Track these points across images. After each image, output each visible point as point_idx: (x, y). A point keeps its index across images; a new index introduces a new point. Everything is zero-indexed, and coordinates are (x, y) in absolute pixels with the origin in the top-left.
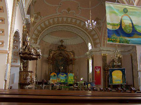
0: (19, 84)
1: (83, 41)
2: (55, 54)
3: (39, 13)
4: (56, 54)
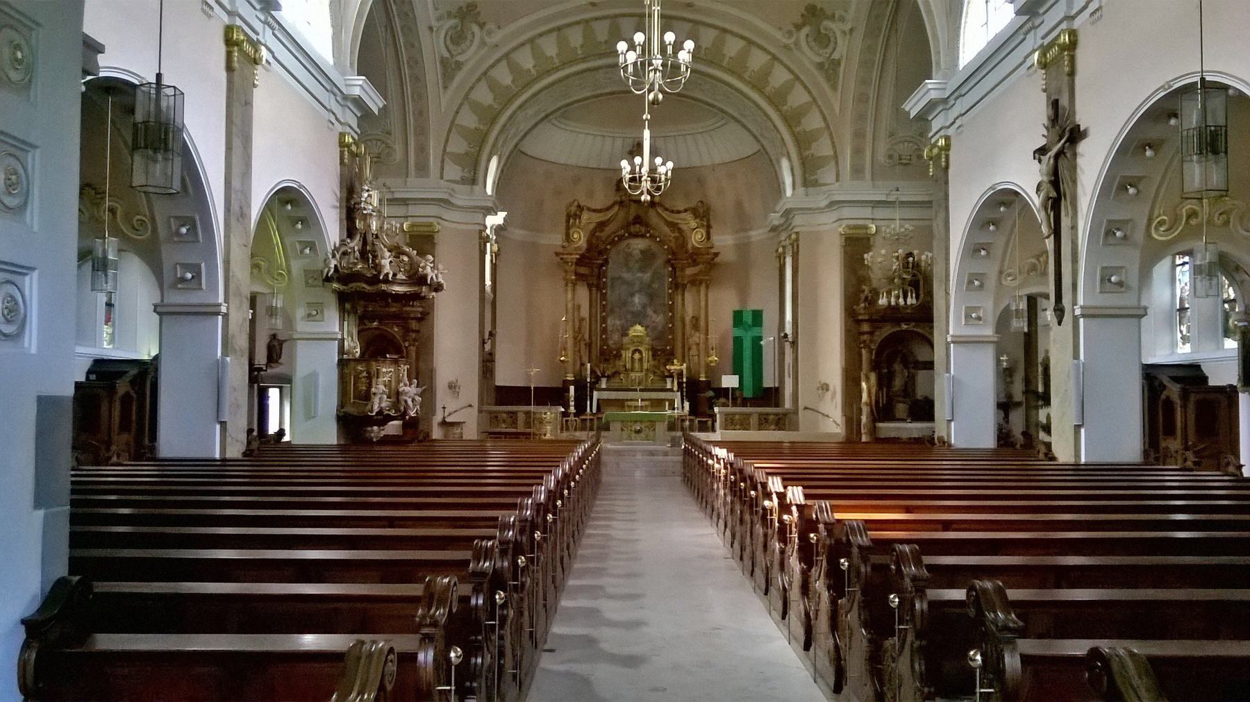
1: (756, 147)
2: (601, 225)
3: (471, 7)
4: (609, 230)
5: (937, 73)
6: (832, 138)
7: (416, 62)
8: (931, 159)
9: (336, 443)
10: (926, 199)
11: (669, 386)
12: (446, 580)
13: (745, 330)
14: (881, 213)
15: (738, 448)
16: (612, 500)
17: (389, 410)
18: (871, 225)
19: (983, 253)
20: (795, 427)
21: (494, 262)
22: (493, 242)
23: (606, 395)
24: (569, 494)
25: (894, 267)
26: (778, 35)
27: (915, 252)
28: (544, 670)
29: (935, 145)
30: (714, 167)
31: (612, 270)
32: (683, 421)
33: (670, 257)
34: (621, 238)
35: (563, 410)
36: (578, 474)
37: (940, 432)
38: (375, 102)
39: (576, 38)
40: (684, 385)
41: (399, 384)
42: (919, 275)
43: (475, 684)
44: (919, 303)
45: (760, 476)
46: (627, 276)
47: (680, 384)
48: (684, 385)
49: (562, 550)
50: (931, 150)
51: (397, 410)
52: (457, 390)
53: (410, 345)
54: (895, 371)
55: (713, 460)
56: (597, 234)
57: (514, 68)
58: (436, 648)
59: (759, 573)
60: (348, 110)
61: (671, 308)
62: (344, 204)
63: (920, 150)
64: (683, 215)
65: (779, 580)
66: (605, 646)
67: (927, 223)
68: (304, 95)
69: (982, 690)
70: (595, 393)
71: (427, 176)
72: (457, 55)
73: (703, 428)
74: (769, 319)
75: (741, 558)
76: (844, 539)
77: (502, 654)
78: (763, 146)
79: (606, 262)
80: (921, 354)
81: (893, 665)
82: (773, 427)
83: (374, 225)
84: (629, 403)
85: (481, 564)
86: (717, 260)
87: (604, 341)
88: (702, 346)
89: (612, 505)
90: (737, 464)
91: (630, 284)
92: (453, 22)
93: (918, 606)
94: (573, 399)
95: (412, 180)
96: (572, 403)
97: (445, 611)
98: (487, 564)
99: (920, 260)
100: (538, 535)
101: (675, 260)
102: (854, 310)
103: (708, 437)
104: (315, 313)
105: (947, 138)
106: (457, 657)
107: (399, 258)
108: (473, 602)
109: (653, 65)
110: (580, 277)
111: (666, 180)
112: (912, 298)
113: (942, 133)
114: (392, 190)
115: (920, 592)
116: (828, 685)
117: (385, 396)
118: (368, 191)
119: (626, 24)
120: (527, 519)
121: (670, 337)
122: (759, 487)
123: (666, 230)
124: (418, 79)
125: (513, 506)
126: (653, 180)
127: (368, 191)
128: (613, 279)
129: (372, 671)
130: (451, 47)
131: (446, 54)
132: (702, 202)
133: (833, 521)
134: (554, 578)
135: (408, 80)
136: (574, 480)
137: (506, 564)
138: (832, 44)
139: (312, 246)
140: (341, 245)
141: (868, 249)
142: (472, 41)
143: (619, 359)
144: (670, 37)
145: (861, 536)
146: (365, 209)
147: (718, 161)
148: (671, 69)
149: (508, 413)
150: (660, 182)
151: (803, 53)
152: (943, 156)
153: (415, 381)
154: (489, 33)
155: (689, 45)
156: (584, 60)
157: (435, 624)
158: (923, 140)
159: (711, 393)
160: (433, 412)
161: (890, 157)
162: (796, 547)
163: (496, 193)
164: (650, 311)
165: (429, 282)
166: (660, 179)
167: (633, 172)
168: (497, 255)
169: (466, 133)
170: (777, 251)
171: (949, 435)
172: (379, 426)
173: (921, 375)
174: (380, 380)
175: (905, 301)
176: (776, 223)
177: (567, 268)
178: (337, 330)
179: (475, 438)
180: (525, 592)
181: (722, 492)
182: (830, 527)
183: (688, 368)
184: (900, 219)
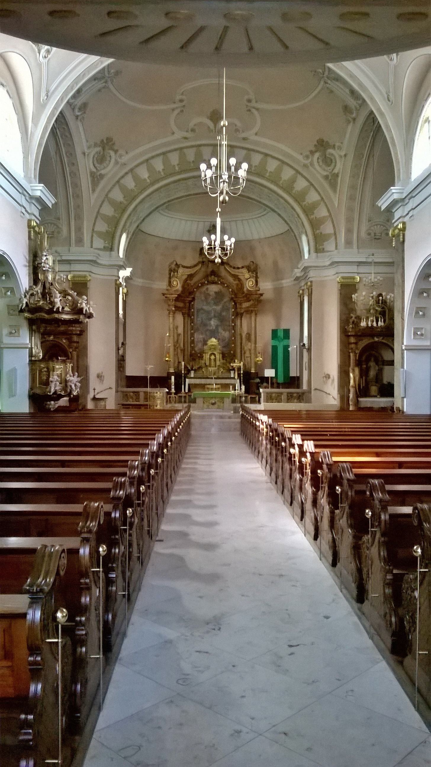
0: (29, 399)
1: (287, 228)
2: (191, 276)
3: (109, 140)
4: (195, 279)
5: (398, 183)
6: (333, 222)
7: (75, 175)
8: (393, 236)
9: (28, 412)
10: (391, 260)
11: (232, 376)
12: (96, 504)
13: (279, 341)
14: (362, 269)
15: (274, 415)
16: (196, 446)
17: (61, 392)
18: (356, 277)
19: (425, 294)
20: (309, 401)
21: (124, 299)
22: (124, 287)
23: (193, 381)
24: (171, 444)
25: (370, 303)
26: (300, 158)
27: (384, 294)
28: (157, 553)
29: (396, 227)
30: (260, 240)
31: (197, 304)
32: (241, 397)
33: (233, 296)
34: (203, 284)
35: (167, 390)
36: (177, 432)
37: (397, 404)
38: (50, 200)
39: (174, 158)
40: (242, 375)
41: (66, 375)
42: (386, 307)
43: (114, 565)
44: (386, 324)
45: (288, 434)
46: (205, 308)
47: (239, 375)
48: (242, 375)
49: (167, 479)
50: (394, 231)
51: (66, 391)
52: (102, 378)
53: (73, 351)
54: (370, 366)
55: (259, 422)
56: (188, 282)
57: (136, 178)
58: (90, 546)
59: (287, 493)
60: (33, 205)
61: (234, 328)
62: (31, 264)
63: (387, 230)
64: (240, 270)
65: (299, 497)
66: (193, 538)
67: (391, 275)
68: (6, 196)
69: (421, 570)
70: (187, 380)
71: (83, 246)
72: (101, 170)
73: (253, 401)
74: (294, 334)
75: (276, 483)
76: (338, 475)
77: (130, 545)
78: (291, 228)
79: (194, 299)
80: (386, 356)
81: (368, 552)
82: (295, 401)
83: (50, 277)
84: (208, 386)
85: (117, 492)
86: (262, 298)
87: (193, 348)
88: (253, 351)
89: (198, 449)
90: (274, 426)
91: (208, 312)
92: (98, 149)
93: (383, 517)
94: (173, 384)
95: (74, 249)
96: (173, 387)
97: (96, 523)
98: (121, 492)
99: (386, 298)
100: (152, 472)
101: (236, 298)
102: (346, 329)
103: (256, 407)
104: (14, 331)
105: (404, 223)
106: (104, 551)
107: (66, 297)
108: (113, 515)
109: (222, 178)
110: (177, 308)
111: (231, 249)
112: (381, 321)
113: (400, 220)
114: (61, 254)
115: (384, 508)
116: (329, 563)
117: (58, 383)
118: (46, 256)
119: (206, 151)
120: (145, 462)
121: (233, 345)
122: (287, 440)
123: (231, 279)
124: (76, 185)
125: (137, 453)
126: (223, 249)
127: (46, 256)
128: (198, 311)
129: (52, 565)
130: (97, 165)
131: (94, 170)
132: (253, 262)
133: (332, 463)
134: (162, 497)
135: (70, 185)
136: (175, 436)
137: (133, 491)
138: (333, 164)
139: (12, 290)
140: (29, 289)
141: (355, 291)
142: (110, 161)
143: (202, 359)
144: (233, 161)
145: (349, 474)
146: (44, 267)
147: (262, 236)
148: (234, 180)
149: (134, 392)
150: (227, 250)
151: (315, 169)
152: (401, 234)
153: (76, 373)
154: (121, 156)
155: (245, 166)
156: (179, 173)
157: (90, 531)
158: (389, 224)
159: (258, 380)
160: (88, 392)
161: (369, 234)
162: (309, 478)
163: (126, 256)
164: (220, 330)
165: (84, 313)
166: (227, 248)
167: (210, 244)
168: (126, 294)
169: (107, 219)
170: (299, 292)
171: (403, 406)
172: (54, 401)
173: (387, 368)
174: (55, 373)
175: (377, 324)
176: (298, 275)
177: (170, 303)
178: (28, 342)
179: (113, 408)
180: (145, 506)
181: (264, 442)
182: (329, 467)
183: (244, 365)
184: (374, 273)
